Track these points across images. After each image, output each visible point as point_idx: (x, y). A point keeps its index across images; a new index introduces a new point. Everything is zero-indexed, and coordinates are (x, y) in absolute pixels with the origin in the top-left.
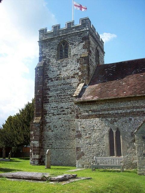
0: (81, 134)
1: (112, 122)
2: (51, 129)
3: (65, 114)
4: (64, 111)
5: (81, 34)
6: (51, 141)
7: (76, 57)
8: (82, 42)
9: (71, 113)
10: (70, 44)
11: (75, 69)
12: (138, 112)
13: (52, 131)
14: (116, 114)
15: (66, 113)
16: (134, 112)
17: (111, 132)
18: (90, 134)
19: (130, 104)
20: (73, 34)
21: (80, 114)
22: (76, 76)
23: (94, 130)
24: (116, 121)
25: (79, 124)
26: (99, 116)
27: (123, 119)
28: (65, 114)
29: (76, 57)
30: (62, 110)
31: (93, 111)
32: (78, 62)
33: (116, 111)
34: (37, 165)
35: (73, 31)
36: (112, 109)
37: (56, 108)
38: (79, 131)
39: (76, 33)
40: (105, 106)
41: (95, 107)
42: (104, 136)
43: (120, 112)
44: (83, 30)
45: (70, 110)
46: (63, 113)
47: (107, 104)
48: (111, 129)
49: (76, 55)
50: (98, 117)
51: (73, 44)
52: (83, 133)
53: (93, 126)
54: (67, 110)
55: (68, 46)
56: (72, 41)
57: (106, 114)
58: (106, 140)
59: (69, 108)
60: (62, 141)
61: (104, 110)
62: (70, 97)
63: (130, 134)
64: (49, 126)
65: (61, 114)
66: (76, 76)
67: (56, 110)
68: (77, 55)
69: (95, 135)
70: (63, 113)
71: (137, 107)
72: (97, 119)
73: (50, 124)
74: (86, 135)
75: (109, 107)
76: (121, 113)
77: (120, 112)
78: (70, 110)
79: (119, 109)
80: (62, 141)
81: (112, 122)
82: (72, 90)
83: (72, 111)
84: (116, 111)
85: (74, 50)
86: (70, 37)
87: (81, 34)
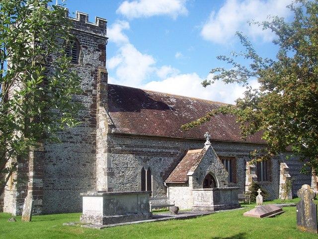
0: (113, 172)
1: (145, 161)
2: (52, 162)
3: (73, 142)
4: (71, 138)
5: (98, 39)
6: (51, 179)
7: (90, 67)
8: (99, 51)
9: (81, 142)
10: (83, 47)
11: (87, 84)
12: (167, 153)
13: (54, 165)
14: (148, 152)
15: (75, 141)
16: (163, 152)
17: (143, 172)
18: (123, 172)
19: (161, 144)
20: (88, 33)
21: (113, 147)
22: (88, 94)
23: (127, 167)
24: (148, 160)
25: (112, 160)
26: (133, 153)
27: (155, 158)
28: (73, 142)
29: (90, 67)
30: (69, 135)
31: (127, 146)
32: (92, 76)
33: (149, 149)
34: (40, 215)
35: (87, 29)
36: (145, 147)
37: (60, 132)
38: (111, 168)
39: (92, 34)
40: (139, 143)
41: (128, 142)
42: (137, 175)
43: (152, 150)
44: (100, 35)
45: (79, 138)
46: (71, 140)
47: (141, 140)
48: (143, 168)
49: (89, 65)
50: (131, 154)
51: (87, 48)
52: (116, 171)
53: (127, 164)
54: (76, 137)
55: (80, 49)
56: (85, 43)
57: (140, 151)
58: (139, 180)
59: (78, 135)
60: (69, 180)
61: (138, 147)
62: (80, 119)
63: (159, 174)
64: (49, 157)
65: (67, 142)
66: (88, 94)
67: (60, 135)
68: (92, 65)
69: (129, 173)
70: (71, 140)
71: (166, 148)
72: (131, 156)
73: (51, 154)
74: (119, 173)
75: (142, 144)
76: (153, 152)
77: (152, 150)
78: (79, 138)
79: (151, 147)
80: (69, 180)
81: (145, 161)
82: (83, 111)
83: (82, 140)
84: (149, 149)
85: (88, 56)
86: (83, 36)
87: (98, 39)
